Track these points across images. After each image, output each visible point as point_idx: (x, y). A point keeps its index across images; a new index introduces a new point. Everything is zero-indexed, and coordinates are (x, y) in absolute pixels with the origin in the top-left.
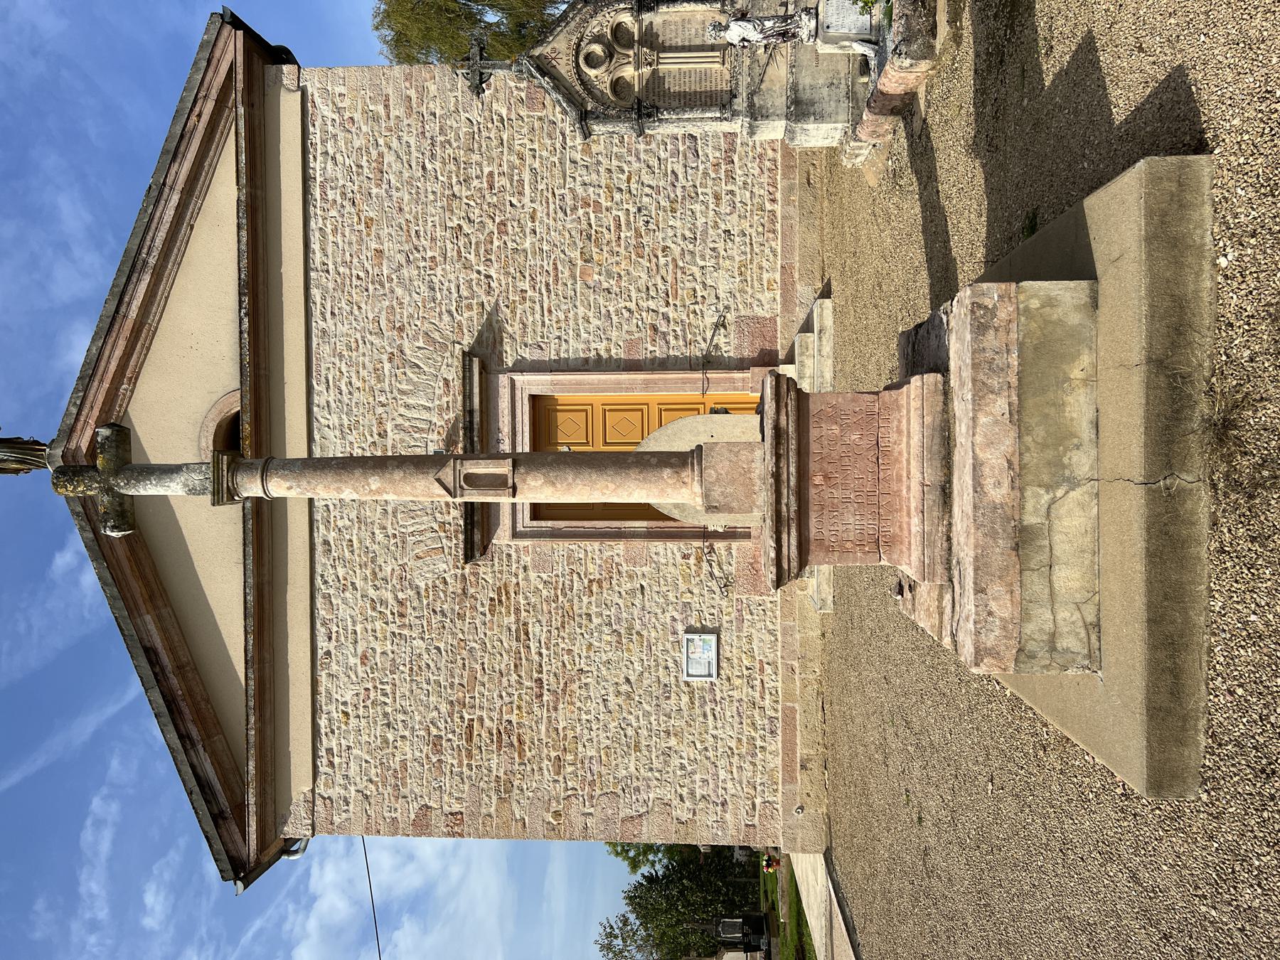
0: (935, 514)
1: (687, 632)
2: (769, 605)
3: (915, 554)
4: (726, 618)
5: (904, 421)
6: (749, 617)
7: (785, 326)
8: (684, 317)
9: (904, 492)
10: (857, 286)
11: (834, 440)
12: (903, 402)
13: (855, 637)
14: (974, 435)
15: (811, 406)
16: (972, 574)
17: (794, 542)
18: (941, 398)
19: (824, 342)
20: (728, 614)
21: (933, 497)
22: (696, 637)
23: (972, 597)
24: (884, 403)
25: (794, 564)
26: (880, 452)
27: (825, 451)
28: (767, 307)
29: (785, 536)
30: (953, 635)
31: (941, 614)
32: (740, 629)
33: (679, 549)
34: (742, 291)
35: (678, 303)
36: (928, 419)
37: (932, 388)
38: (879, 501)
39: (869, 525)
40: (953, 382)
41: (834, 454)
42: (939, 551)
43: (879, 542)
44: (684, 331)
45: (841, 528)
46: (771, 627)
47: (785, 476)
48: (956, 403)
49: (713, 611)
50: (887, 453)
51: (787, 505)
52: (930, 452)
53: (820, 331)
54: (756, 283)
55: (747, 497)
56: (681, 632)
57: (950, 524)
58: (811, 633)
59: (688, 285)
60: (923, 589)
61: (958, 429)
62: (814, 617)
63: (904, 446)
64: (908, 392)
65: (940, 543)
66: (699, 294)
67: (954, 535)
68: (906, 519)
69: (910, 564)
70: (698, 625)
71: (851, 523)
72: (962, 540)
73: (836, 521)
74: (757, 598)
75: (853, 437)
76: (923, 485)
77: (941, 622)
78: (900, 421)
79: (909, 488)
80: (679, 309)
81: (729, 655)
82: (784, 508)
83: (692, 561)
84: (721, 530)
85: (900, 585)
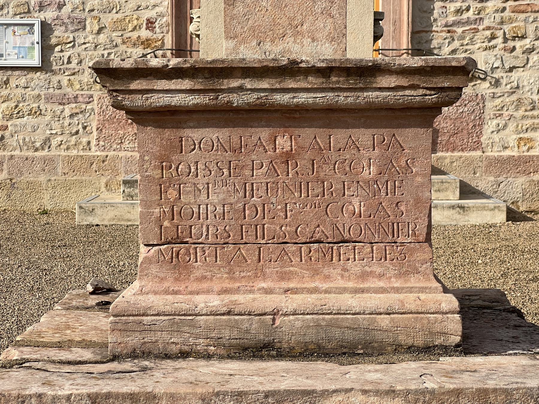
0: (226, 333)
1: (44, 25)
2: (85, 140)
3: (158, 302)
4: (65, 81)
5: (381, 284)
6: (67, 113)
7: (469, 162)
8: (487, 23)
9: (264, 285)
10: (530, 252)
11: (351, 169)
12: (414, 282)
13: (39, 252)
14: (365, 392)
15: (410, 132)
16: (125, 390)
17: (177, 100)
18: (419, 342)
19: (447, 213)
20: (71, 84)
21: (255, 329)
22: (37, 37)
23: (85, 391)
24: (412, 251)
25: (139, 101)
26: (329, 245)
27: (333, 155)
28: (496, 137)
29: (186, 84)
30: (20, 363)
31: (60, 345)
32: (49, 99)
33: (161, 15)
34: (519, 103)
35: (507, 14)
36: (384, 321)
37: (437, 328)
38: (246, 242)
39: (206, 228)
40: (449, 362)
41: (327, 169)
42: (163, 339)
43: (176, 243)
44: (468, 22)
45: (201, 181)
46: (54, 142)
47: (291, 84)
48: (413, 365)
49: (75, 61)
50: (328, 258)
51: (241, 89)
52: (331, 325)
53: (462, 207)
54: (529, 122)
55: (253, 29)
56: (42, 16)
57: (209, 357)
58: (47, 197)
59: (531, 29)
60: (103, 321)
61: (371, 367)
62: (71, 201)
63: (341, 283)
64: (429, 290)
65: (177, 341)
66: (518, 44)
67: (191, 363)
68: (217, 287)
69: (141, 292)
70: (53, 41)
71: (210, 198)
72: (184, 375)
73: (212, 170)
74: (94, 125)
75: (356, 202)
76: (275, 313)
77: (46, 345)
78: (381, 276)
79: (268, 291)
80: (498, 16)
81: (13, 83)
82: (235, 83)
83: (144, 33)
84: (192, 28)
85: (110, 290)
